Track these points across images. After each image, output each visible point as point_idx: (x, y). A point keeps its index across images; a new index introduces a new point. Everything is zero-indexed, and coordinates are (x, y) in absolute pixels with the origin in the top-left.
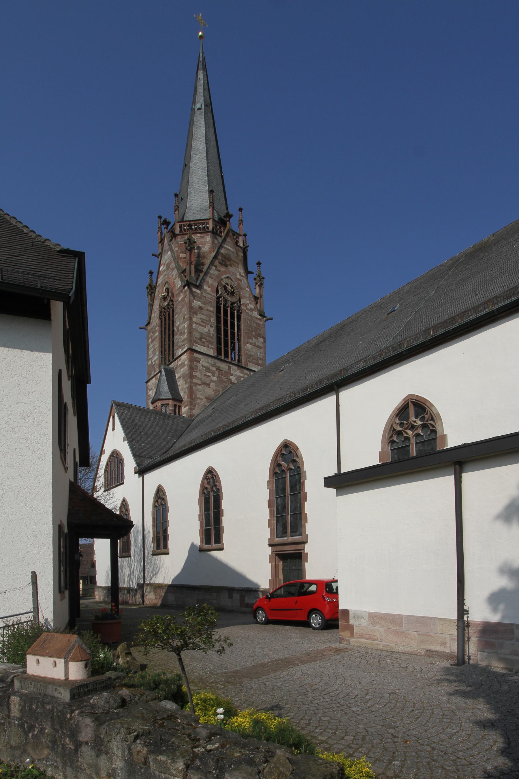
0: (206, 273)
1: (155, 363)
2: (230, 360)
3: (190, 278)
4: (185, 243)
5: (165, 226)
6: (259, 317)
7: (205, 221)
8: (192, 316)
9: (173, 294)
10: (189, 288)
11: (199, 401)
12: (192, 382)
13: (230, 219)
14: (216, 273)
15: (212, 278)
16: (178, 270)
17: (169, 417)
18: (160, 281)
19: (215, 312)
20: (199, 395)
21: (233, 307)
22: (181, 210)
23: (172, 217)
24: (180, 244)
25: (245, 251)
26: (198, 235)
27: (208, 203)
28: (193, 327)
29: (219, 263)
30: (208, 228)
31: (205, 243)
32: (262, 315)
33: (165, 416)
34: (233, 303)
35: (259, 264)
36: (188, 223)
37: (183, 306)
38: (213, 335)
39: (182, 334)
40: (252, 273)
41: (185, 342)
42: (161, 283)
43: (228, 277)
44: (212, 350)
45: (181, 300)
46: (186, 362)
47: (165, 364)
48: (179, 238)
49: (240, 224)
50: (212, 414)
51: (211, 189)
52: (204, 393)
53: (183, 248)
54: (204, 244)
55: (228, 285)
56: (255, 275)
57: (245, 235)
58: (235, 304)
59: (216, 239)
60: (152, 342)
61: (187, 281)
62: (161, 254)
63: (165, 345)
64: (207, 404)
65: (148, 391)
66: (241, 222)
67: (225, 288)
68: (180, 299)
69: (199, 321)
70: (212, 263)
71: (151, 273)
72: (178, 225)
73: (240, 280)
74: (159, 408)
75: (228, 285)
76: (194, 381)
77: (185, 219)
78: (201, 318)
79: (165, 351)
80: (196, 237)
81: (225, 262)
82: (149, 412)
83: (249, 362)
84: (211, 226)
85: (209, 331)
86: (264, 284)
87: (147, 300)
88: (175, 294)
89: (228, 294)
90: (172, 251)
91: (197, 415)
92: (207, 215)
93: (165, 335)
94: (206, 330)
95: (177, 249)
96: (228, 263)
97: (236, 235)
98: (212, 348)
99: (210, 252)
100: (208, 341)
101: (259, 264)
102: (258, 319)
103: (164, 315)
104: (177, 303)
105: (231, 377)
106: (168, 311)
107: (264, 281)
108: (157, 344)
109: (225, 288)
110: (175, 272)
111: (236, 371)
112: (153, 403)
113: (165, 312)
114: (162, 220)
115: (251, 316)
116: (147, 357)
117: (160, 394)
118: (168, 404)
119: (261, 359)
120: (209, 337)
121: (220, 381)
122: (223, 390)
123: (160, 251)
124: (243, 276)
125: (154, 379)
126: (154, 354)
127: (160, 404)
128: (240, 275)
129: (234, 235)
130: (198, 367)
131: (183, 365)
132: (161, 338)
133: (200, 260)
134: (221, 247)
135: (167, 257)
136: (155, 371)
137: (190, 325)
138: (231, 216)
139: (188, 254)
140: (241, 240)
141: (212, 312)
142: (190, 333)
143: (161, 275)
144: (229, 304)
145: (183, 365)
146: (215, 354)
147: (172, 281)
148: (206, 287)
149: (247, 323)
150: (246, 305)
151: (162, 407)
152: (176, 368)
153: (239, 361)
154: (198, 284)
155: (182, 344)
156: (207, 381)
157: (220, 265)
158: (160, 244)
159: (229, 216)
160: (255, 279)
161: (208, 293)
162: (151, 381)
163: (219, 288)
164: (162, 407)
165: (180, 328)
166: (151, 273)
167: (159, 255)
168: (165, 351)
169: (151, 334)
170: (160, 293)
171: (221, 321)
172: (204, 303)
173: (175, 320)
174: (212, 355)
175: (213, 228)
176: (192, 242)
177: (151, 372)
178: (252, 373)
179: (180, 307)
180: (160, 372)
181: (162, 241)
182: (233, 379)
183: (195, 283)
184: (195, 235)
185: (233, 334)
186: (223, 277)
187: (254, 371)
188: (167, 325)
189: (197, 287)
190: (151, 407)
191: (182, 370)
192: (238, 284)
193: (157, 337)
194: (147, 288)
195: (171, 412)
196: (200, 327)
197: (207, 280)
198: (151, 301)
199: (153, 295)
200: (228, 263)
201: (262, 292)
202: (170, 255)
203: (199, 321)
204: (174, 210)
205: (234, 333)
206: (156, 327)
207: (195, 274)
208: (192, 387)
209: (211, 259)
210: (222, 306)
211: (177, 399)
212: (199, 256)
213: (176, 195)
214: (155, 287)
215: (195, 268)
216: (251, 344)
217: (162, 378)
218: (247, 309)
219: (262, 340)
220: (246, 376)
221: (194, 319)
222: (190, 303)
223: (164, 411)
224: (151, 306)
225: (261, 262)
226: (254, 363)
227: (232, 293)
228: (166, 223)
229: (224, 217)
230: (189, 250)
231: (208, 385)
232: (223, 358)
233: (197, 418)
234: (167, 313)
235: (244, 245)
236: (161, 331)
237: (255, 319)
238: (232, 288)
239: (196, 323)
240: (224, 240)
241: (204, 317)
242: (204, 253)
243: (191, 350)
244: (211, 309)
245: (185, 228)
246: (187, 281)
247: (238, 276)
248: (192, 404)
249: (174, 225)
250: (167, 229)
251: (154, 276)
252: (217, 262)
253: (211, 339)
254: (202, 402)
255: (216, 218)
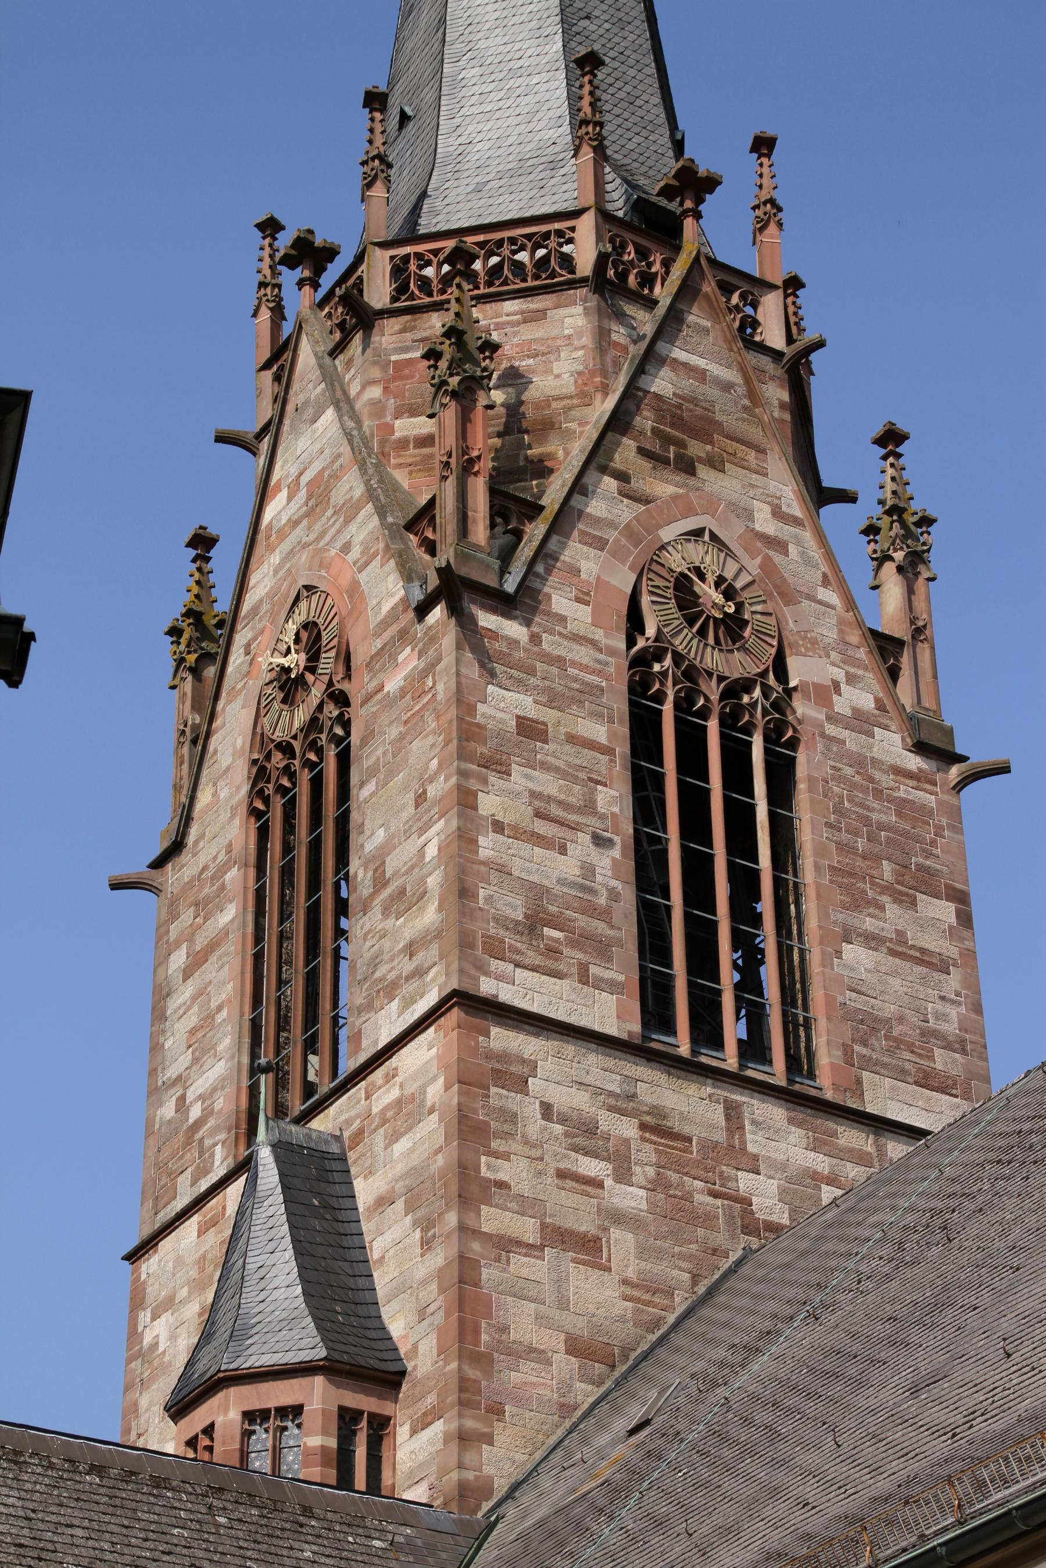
0: (564, 520)
1: (207, 1113)
2: (730, 1060)
3: (461, 556)
4: (433, 355)
5: (303, 272)
6: (914, 762)
7: (549, 228)
8: (473, 784)
9: (346, 658)
10: (455, 610)
11: (522, 1375)
12: (476, 1233)
13: (700, 201)
14: (626, 512)
15: (600, 544)
16: (381, 512)
17: (307, 1511)
18: (262, 583)
19: (623, 748)
20: (522, 1323)
21: (738, 710)
22: (404, 182)
23: (343, 220)
24: (399, 366)
25: (796, 371)
26: (510, 306)
27: (566, 128)
28: (483, 853)
29: (642, 451)
30: (567, 262)
31: (555, 350)
32: (935, 747)
33: (273, 1501)
34: (734, 690)
35: (891, 439)
36: (450, 244)
37: (413, 726)
38: (614, 895)
39: (404, 901)
40: (847, 497)
41: (433, 952)
42: (272, 594)
43: (698, 533)
44: (608, 1002)
45: (403, 692)
46: (435, 1092)
47: (280, 1111)
48: (388, 335)
49: (762, 226)
50: (634, 1474)
51: (582, 51)
52: (561, 1307)
53: (419, 382)
54: (549, 351)
55: (702, 577)
56: (867, 510)
57: (793, 284)
58: (749, 690)
59: (620, 316)
60: (187, 974)
61: (445, 572)
62: (272, 429)
63: (281, 983)
64: (585, 1394)
65: (144, 1317)
66: (769, 213)
67: (683, 590)
68: (393, 684)
69: (519, 813)
70: (598, 458)
71: (202, 543)
72: (380, 262)
73: (780, 546)
74: (226, 1446)
75: (702, 577)
76: (493, 1219)
77: (427, 224)
78: (534, 795)
79: (282, 1023)
80: (499, 319)
81: (681, 444)
82: (159, 1483)
83: (868, 1064)
84: (585, 248)
85: (589, 870)
86: (932, 556)
87: (172, 708)
88: (358, 659)
89: (702, 633)
90: (343, 402)
91: (515, 1487)
92: (566, 187)
93: (284, 916)
94: (567, 867)
95: (375, 392)
96: (696, 449)
97: (740, 285)
98: (613, 987)
99: (585, 398)
100: (582, 940)
101: (891, 439)
102: (909, 775)
103: (282, 790)
104: (372, 707)
105: (745, 1182)
106: (311, 765)
107: (938, 540)
108: (225, 980)
109: (683, 590)
110: (365, 527)
111: (774, 1134)
112: (179, 1408)
113: (288, 771)
114: (284, 241)
115: (860, 762)
116: (153, 1072)
117: (239, 1334)
118: (297, 1410)
119: (948, 1047)
120: (591, 910)
121: (675, 1213)
122: (695, 1279)
123: (267, 411)
124: (796, 522)
125: (191, 1226)
126: (200, 1046)
127: (234, 1415)
128: (777, 513)
129: (727, 289)
130: (512, 1118)
131: (407, 1111)
132: (258, 937)
133: (521, 445)
134: (650, 359)
135: (313, 442)
136: (202, 1171)
137: (465, 839)
138: (711, 183)
139: (450, 414)
140: (770, 315)
141: (608, 751)
142: (462, 891)
143: (270, 549)
144: (713, 691)
145: (407, 1111)
146: (632, 1027)
147: (345, 580)
148: (560, 601)
149: (838, 810)
150: (824, 694)
151: (247, 1434)
152: (359, 1136)
153: (800, 1062)
154: (510, 585)
155: (408, 966)
156: (577, 1213)
157: (646, 465)
158: (268, 375)
159: (693, 185)
160: (871, 530)
161: (576, 638)
162: (166, 1245)
163: (645, 600)
164: (247, 1434)
165: (392, 864)
166: (202, 543)
167: (259, 436)
168: (282, 1023)
169: (187, 916)
170: (258, 652)
171: (662, 803)
172: (553, 700)
173: (355, 816)
174: (612, 1029)
175: (602, 260)
176: (473, 345)
177: (173, 1176)
178: (896, 1149)
179: (394, 732)
180: (245, 1166)
181: (280, 357)
182: (765, 1194)
183: (490, 580)
184: (490, 308)
185: (745, 885)
186: (667, 534)
187: (914, 1133)
188: (302, 854)
189: (505, 604)
190: (166, 1438)
191: (402, 1146)
192: (768, 566)
193: (225, 932)
194: (175, 632)
195: (314, 1473)
196: (524, 848)
197: (566, 556)
198: (196, 707)
199: (210, 672)
200: (696, 449)
201: (920, 604)
202: (335, 430)
203: (519, 813)
204: (359, 183)
205: (756, 874)
206: (223, 870)
207: (493, 525)
208: (475, 1265)
209: (592, 433)
210: (668, 709)
211: (366, 1366)
212: (513, 422)
213: (375, 101)
214: (229, 624)
215: (493, 492)
216: (872, 940)
217: (260, 1215)
218: (833, 718)
219: (946, 911)
220: (853, 1172)
221: (488, 804)
222: (464, 702)
223: (261, 1463)
224: (199, 740)
225: (902, 426)
226: (901, 1075)
227: (733, 627)
228: (309, 254)
229: (667, 192)
230: (454, 394)
231: (589, 1248)
232: (684, 1050)
233: (511, 1511)
234: (305, 777)
235: (790, 340)
236: (260, 896)
237: (886, 780)
238: (729, 594)
239: (498, 827)
240: (671, 323)
241: (550, 785)
242: (548, 401)
243: (470, 1004)
244: (599, 732)
245: (429, 272)
246: (445, 572)
247: (765, 523)
248: (475, 1402)
249: (359, 259)
250: (316, 286)
251: (224, 561)
252: (626, 452)
253: (600, 927)
254: (545, 1381)
255: (618, 202)
